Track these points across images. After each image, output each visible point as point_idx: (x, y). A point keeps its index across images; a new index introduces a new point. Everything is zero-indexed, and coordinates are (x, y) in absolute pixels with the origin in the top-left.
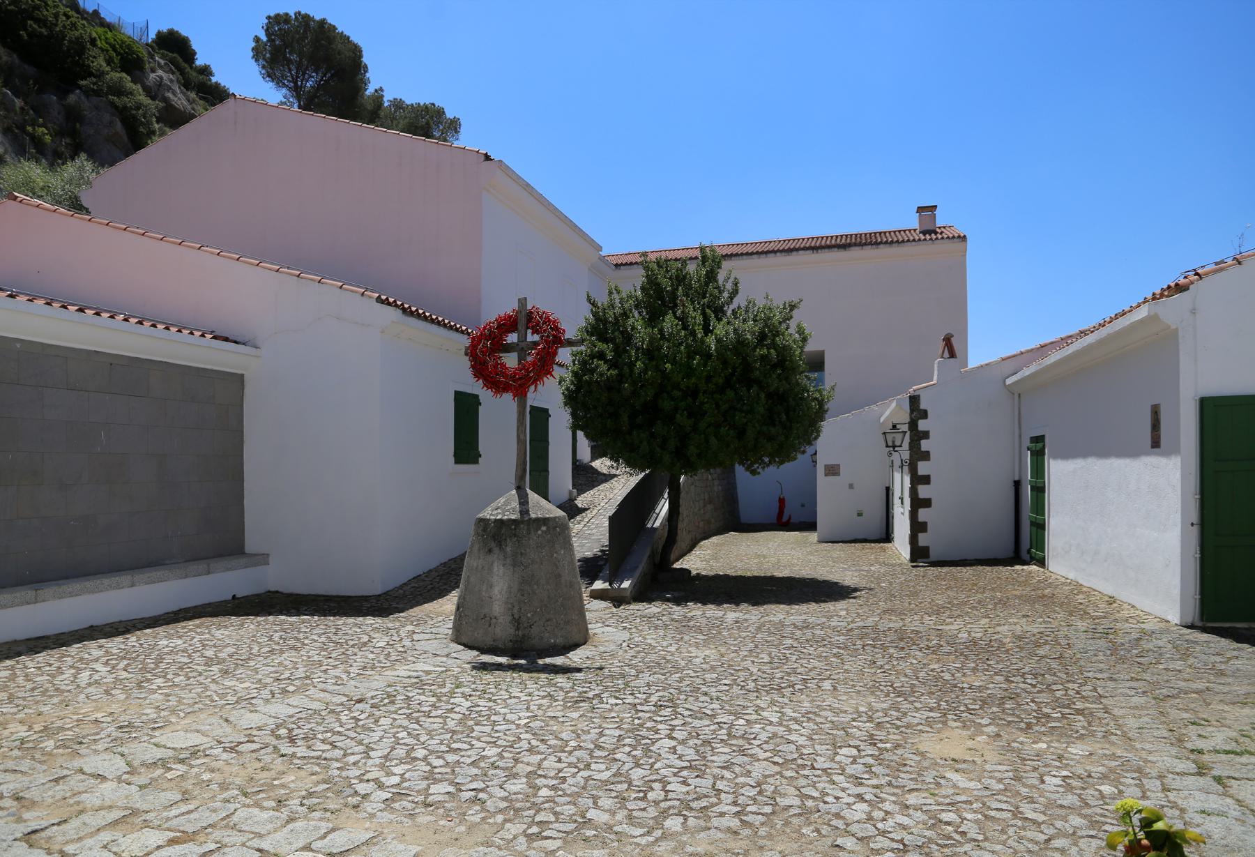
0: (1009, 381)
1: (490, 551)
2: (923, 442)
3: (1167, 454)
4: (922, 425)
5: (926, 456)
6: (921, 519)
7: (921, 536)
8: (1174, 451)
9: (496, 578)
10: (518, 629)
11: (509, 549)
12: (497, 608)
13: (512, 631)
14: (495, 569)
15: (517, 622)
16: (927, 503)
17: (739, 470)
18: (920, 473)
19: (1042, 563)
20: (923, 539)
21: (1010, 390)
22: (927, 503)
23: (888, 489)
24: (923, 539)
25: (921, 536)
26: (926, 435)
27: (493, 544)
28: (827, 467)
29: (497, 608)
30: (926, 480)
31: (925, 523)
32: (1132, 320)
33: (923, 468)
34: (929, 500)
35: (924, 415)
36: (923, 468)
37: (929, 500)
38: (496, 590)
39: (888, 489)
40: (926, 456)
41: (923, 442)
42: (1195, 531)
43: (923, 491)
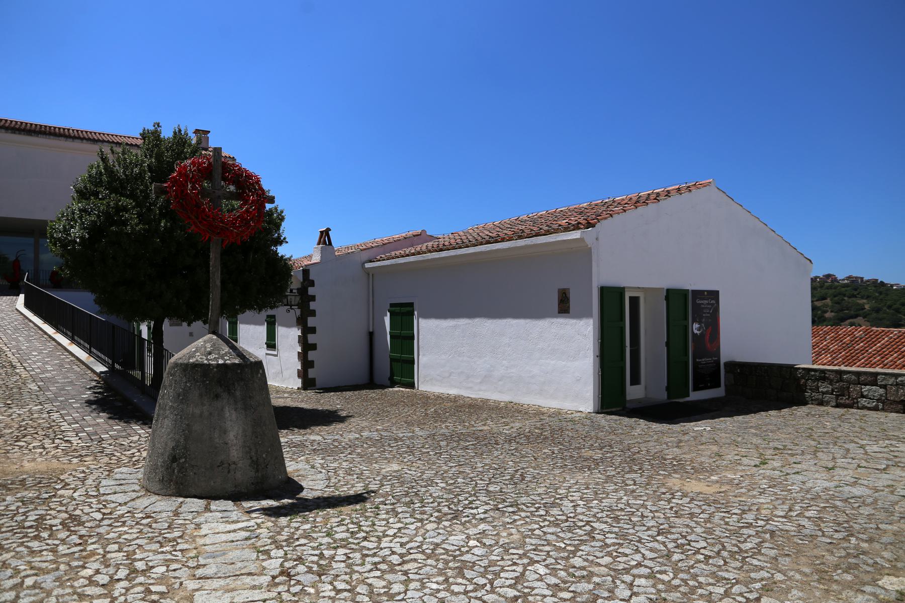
0: (367, 265)
1: (217, 396)
2: (311, 303)
3: (579, 316)
4: (311, 291)
5: (313, 313)
6: (310, 358)
7: (310, 370)
8: (583, 314)
9: (229, 423)
10: (257, 471)
11: (238, 393)
12: (235, 454)
13: (252, 474)
14: (227, 414)
15: (255, 464)
16: (314, 347)
17: (166, 322)
18: (309, 325)
19: (411, 385)
20: (311, 373)
21: (369, 273)
22: (314, 347)
23: (371, 335)
24: (311, 373)
25: (310, 370)
26: (313, 298)
27: (219, 390)
28: (274, 317)
29: (235, 454)
30: (313, 330)
31: (313, 361)
32: (565, 239)
33: (311, 322)
34: (315, 345)
35: (312, 284)
36: (311, 322)
37: (315, 345)
38: (231, 435)
39: (371, 335)
40: (313, 313)
41: (311, 303)
42: (598, 360)
43: (311, 339)
